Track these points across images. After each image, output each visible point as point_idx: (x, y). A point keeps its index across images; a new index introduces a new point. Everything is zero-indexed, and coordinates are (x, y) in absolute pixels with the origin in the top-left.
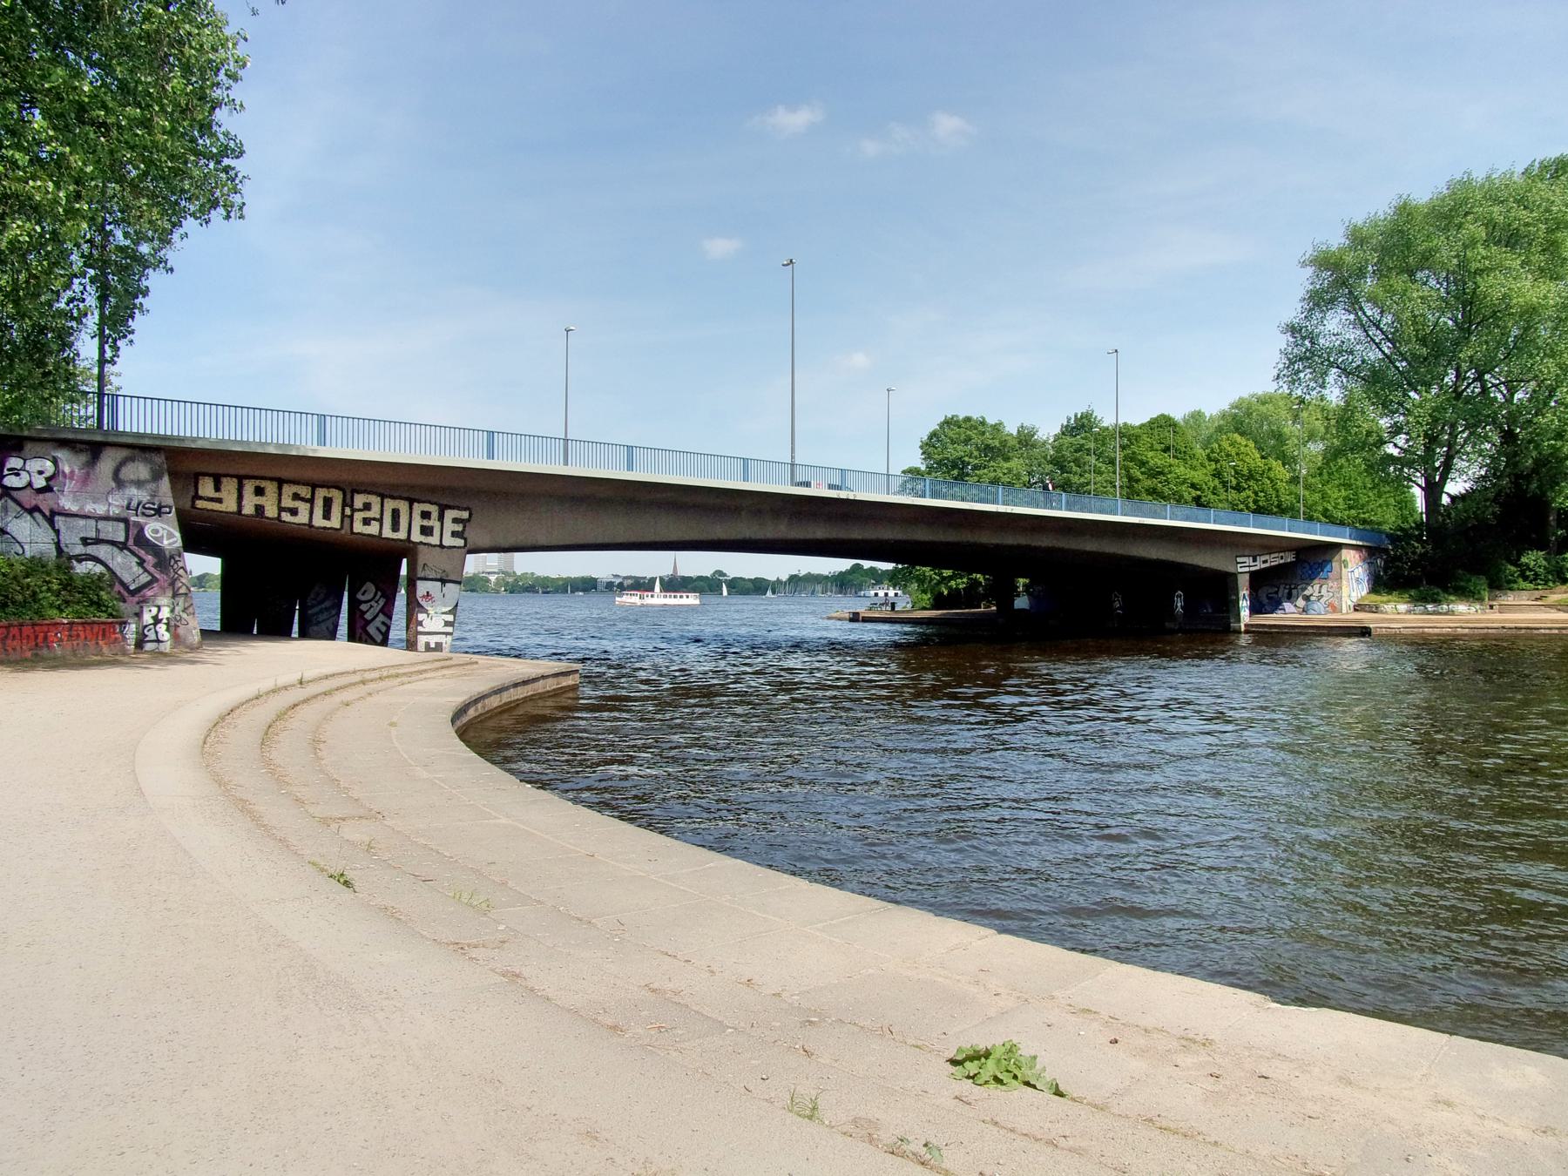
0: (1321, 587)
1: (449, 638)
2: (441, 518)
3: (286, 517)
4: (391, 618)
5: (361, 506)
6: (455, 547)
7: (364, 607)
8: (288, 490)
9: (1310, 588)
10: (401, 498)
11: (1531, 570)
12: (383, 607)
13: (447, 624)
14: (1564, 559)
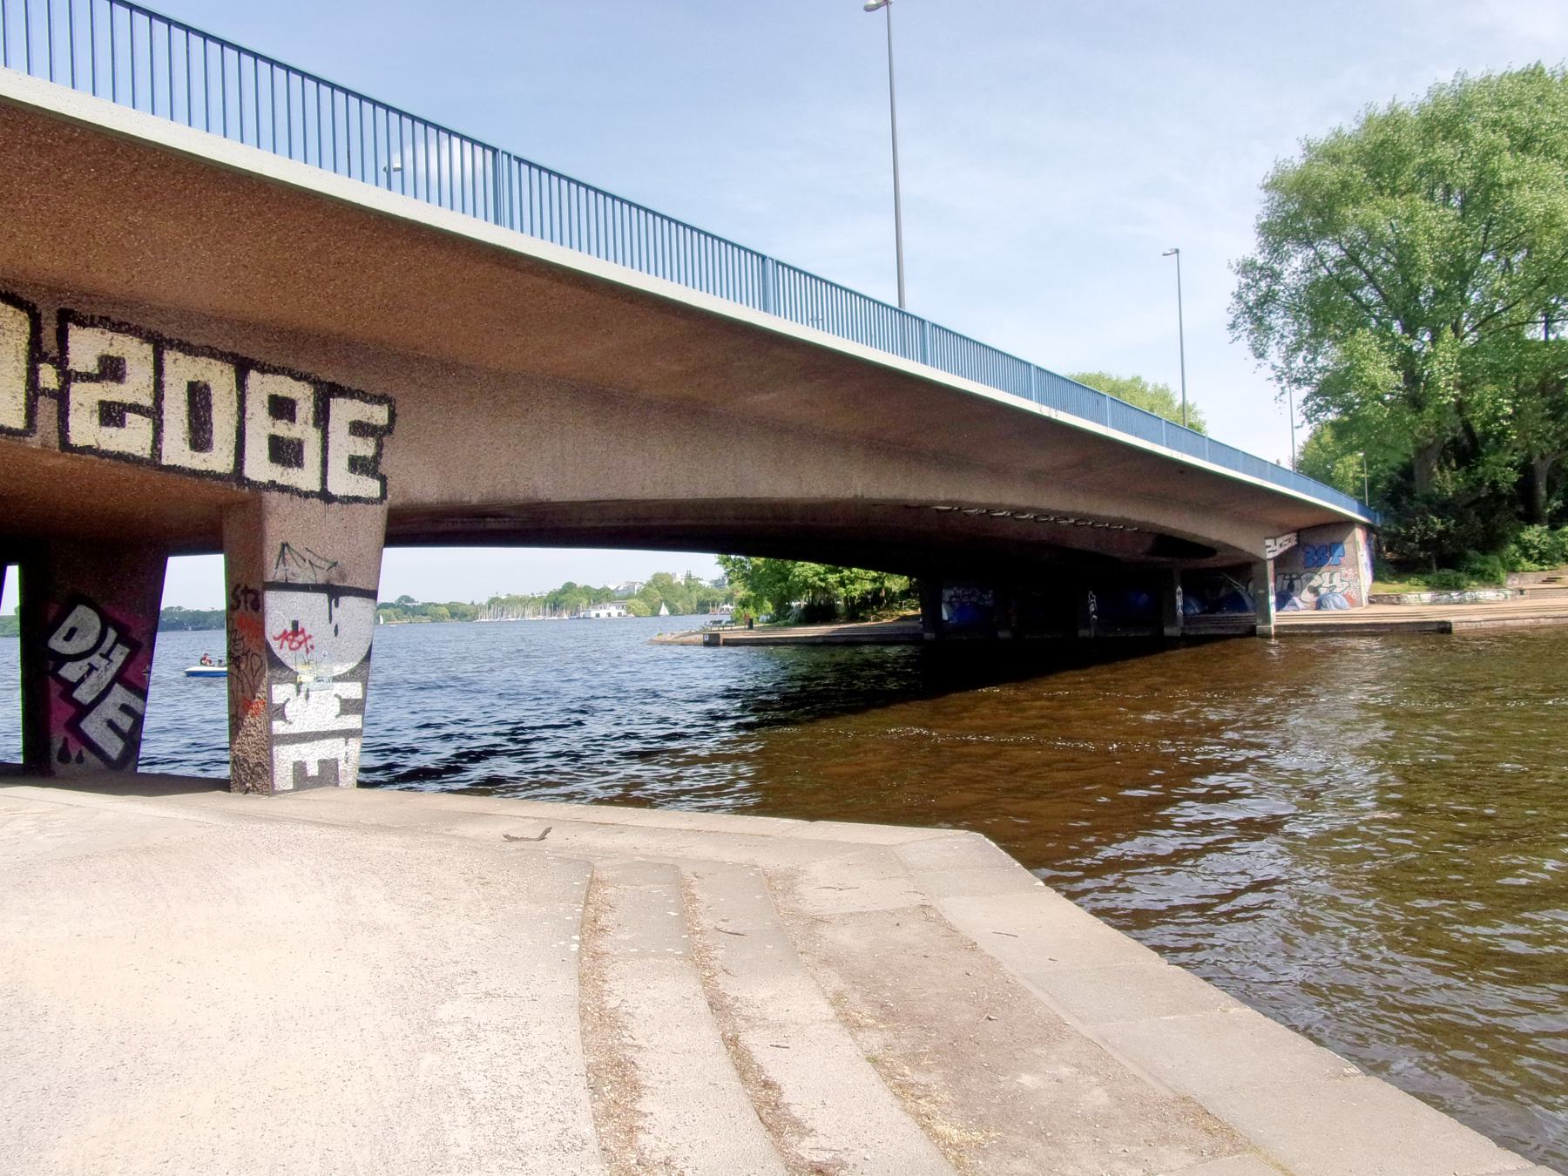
0: (1332, 575)
2: (322, 418)
4: (143, 694)
5: (92, 366)
6: (357, 499)
7: (71, 672)
9: (1317, 577)
10: (213, 353)
11: (1535, 548)
13: (348, 707)
14: (1563, 535)
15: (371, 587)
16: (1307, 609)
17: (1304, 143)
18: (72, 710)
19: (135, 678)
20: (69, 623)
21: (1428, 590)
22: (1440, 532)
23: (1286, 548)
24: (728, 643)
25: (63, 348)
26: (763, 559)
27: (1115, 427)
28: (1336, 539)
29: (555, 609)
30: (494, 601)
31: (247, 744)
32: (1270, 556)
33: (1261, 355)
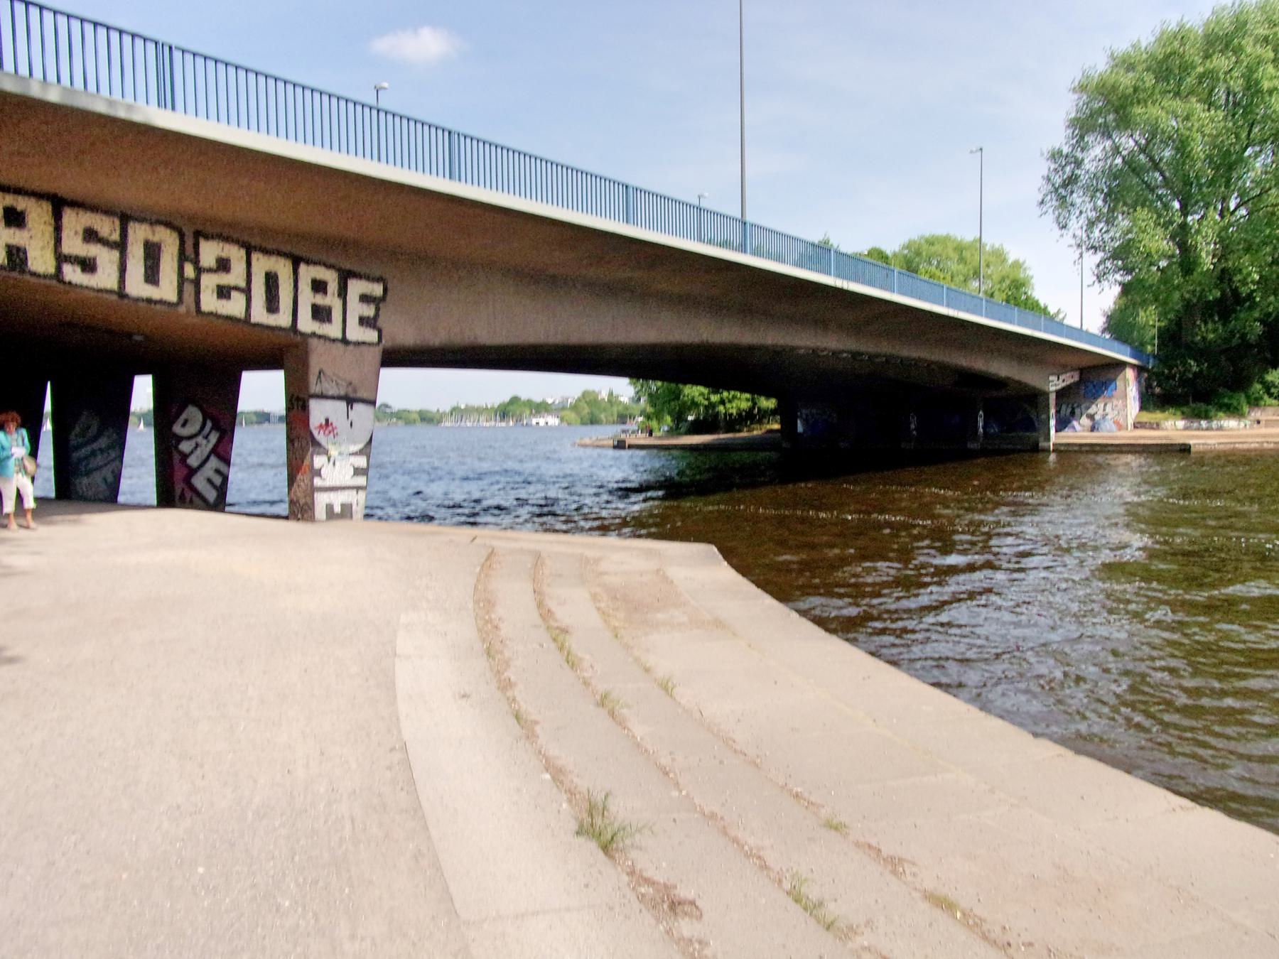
0: (1105, 405)
1: (362, 495)
2: (343, 292)
3: (72, 274)
4: (227, 462)
6: (364, 343)
7: (185, 447)
8: (74, 221)
9: (1094, 406)
10: (280, 253)
12: (216, 446)
13: (358, 471)
15: (371, 398)
16: (1083, 431)
17: (1109, 52)
18: (185, 471)
19: (222, 452)
20: (183, 417)
21: (1183, 419)
22: (1195, 373)
23: (1068, 383)
24: (630, 447)
25: (197, 253)
26: (659, 383)
27: (901, 293)
28: (1110, 376)
29: (504, 417)
30: (455, 410)
31: (299, 492)
32: (1052, 389)
33: (1064, 227)
